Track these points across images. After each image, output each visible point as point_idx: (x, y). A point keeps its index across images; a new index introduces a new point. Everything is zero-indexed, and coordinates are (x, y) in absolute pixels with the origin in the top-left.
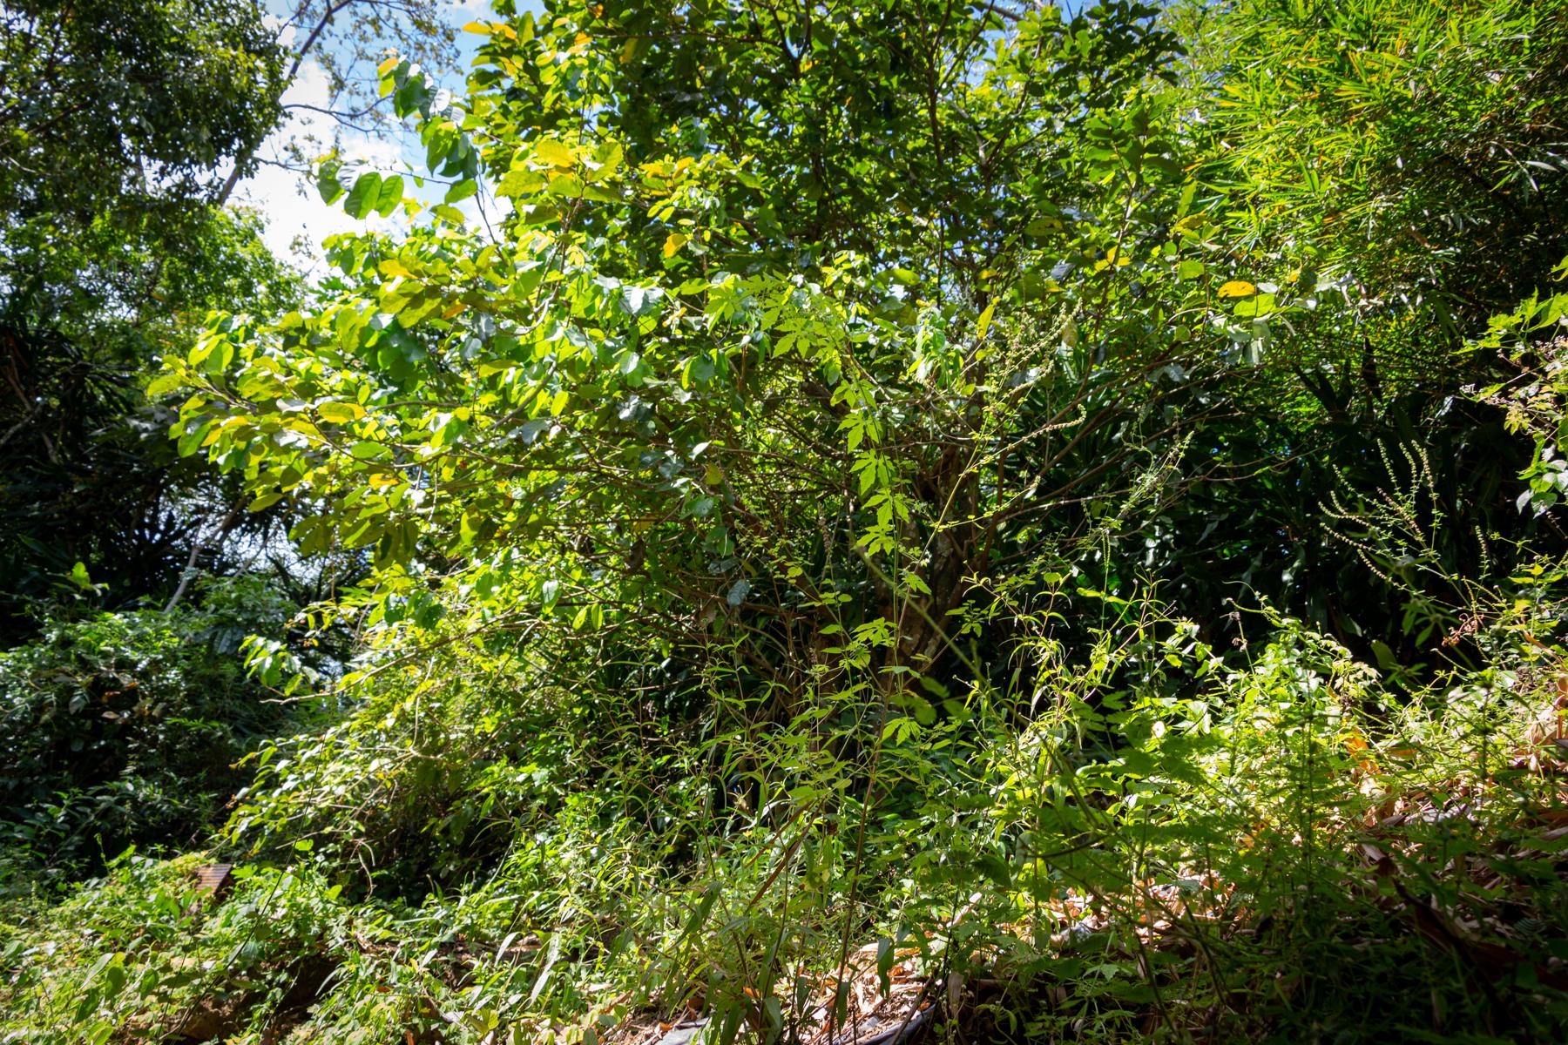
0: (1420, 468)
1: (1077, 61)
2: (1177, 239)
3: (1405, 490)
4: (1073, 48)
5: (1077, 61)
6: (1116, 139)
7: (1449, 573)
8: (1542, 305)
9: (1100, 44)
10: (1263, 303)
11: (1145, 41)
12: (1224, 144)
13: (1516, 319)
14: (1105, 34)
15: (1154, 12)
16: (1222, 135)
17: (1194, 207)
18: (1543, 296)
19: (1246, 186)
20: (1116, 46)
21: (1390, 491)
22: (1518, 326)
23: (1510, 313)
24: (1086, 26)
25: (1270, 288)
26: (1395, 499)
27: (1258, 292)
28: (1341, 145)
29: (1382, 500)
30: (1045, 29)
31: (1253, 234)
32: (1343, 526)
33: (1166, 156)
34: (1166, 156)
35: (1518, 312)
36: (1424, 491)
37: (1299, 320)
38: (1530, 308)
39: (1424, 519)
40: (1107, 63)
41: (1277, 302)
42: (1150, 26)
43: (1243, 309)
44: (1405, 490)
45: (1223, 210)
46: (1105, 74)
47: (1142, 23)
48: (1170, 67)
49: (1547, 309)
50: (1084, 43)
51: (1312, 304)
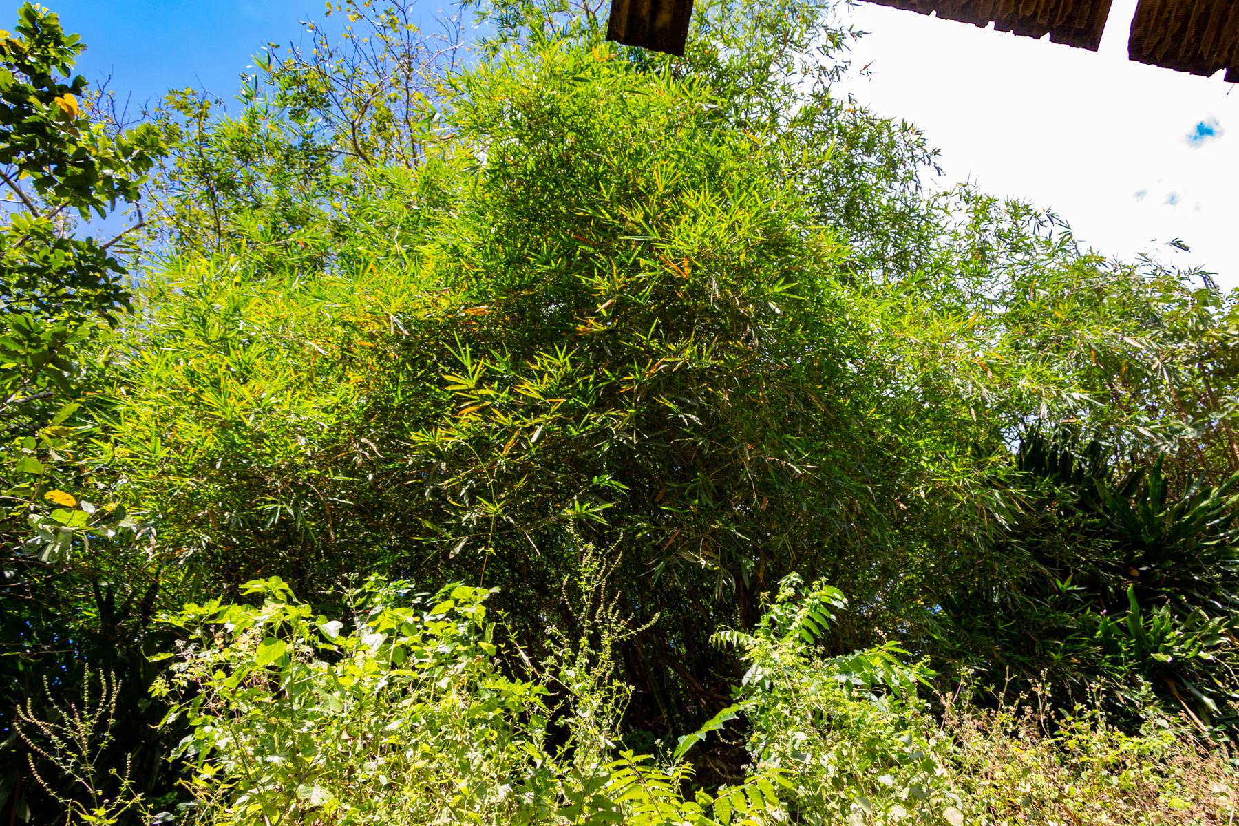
0: (109, 696)
1: (46, 268)
2: (39, 441)
3: (92, 711)
4: (46, 258)
5: (46, 268)
6: (31, 340)
7: (96, 788)
8: (223, 608)
9: (70, 268)
10: (77, 518)
11: (106, 286)
12: (123, 389)
13: (202, 611)
14: (78, 264)
15: (123, 271)
16: (126, 383)
17: (71, 421)
18: (226, 602)
19: (118, 427)
20: (82, 277)
21: (80, 705)
22: (201, 617)
23: (200, 605)
24: (66, 250)
25: (90, 509)
26: (81, 716)
27: (79, 507)
28: (190, 431)
29: (71, 715)
30: (33, 232)
31: (102, 460)
32: (31, 730)
33: (66, 374)
34: (66, 374)
35: (206, 607)
36: (106, 715)
37: (99, 542)
38: (213, 607)
39: (94, 742)
40: (68, 283)
41: (88, 521)
42: (115, 279)
43: (59, 515)
44: (92, 711)
45: (92, 435)
46: (63, 291)
47: (111, 274)
48: (116, 315)
49: (225, 612)
50: (59, 260)
51: (111, 534)
